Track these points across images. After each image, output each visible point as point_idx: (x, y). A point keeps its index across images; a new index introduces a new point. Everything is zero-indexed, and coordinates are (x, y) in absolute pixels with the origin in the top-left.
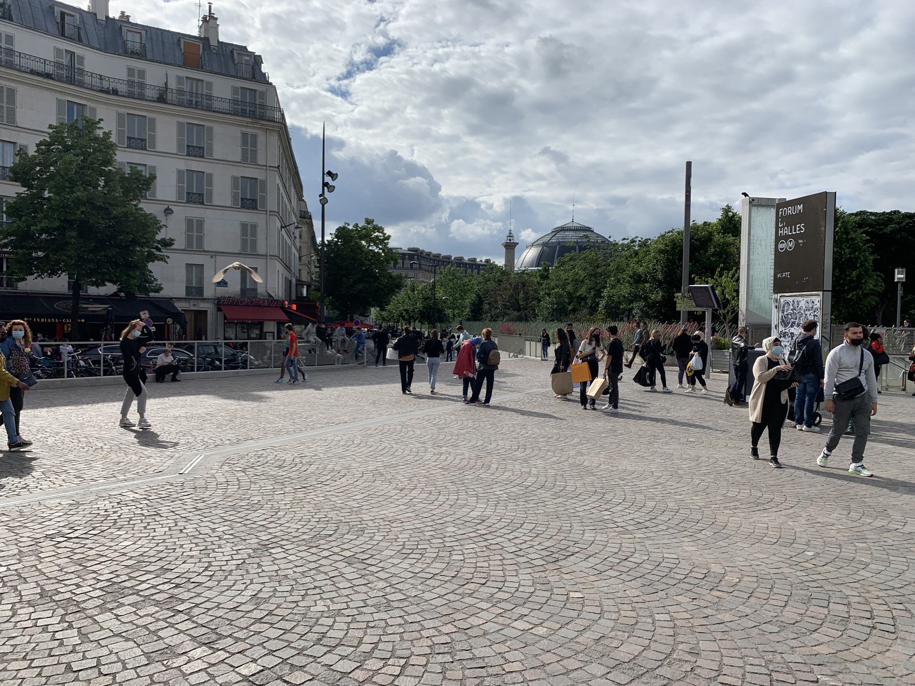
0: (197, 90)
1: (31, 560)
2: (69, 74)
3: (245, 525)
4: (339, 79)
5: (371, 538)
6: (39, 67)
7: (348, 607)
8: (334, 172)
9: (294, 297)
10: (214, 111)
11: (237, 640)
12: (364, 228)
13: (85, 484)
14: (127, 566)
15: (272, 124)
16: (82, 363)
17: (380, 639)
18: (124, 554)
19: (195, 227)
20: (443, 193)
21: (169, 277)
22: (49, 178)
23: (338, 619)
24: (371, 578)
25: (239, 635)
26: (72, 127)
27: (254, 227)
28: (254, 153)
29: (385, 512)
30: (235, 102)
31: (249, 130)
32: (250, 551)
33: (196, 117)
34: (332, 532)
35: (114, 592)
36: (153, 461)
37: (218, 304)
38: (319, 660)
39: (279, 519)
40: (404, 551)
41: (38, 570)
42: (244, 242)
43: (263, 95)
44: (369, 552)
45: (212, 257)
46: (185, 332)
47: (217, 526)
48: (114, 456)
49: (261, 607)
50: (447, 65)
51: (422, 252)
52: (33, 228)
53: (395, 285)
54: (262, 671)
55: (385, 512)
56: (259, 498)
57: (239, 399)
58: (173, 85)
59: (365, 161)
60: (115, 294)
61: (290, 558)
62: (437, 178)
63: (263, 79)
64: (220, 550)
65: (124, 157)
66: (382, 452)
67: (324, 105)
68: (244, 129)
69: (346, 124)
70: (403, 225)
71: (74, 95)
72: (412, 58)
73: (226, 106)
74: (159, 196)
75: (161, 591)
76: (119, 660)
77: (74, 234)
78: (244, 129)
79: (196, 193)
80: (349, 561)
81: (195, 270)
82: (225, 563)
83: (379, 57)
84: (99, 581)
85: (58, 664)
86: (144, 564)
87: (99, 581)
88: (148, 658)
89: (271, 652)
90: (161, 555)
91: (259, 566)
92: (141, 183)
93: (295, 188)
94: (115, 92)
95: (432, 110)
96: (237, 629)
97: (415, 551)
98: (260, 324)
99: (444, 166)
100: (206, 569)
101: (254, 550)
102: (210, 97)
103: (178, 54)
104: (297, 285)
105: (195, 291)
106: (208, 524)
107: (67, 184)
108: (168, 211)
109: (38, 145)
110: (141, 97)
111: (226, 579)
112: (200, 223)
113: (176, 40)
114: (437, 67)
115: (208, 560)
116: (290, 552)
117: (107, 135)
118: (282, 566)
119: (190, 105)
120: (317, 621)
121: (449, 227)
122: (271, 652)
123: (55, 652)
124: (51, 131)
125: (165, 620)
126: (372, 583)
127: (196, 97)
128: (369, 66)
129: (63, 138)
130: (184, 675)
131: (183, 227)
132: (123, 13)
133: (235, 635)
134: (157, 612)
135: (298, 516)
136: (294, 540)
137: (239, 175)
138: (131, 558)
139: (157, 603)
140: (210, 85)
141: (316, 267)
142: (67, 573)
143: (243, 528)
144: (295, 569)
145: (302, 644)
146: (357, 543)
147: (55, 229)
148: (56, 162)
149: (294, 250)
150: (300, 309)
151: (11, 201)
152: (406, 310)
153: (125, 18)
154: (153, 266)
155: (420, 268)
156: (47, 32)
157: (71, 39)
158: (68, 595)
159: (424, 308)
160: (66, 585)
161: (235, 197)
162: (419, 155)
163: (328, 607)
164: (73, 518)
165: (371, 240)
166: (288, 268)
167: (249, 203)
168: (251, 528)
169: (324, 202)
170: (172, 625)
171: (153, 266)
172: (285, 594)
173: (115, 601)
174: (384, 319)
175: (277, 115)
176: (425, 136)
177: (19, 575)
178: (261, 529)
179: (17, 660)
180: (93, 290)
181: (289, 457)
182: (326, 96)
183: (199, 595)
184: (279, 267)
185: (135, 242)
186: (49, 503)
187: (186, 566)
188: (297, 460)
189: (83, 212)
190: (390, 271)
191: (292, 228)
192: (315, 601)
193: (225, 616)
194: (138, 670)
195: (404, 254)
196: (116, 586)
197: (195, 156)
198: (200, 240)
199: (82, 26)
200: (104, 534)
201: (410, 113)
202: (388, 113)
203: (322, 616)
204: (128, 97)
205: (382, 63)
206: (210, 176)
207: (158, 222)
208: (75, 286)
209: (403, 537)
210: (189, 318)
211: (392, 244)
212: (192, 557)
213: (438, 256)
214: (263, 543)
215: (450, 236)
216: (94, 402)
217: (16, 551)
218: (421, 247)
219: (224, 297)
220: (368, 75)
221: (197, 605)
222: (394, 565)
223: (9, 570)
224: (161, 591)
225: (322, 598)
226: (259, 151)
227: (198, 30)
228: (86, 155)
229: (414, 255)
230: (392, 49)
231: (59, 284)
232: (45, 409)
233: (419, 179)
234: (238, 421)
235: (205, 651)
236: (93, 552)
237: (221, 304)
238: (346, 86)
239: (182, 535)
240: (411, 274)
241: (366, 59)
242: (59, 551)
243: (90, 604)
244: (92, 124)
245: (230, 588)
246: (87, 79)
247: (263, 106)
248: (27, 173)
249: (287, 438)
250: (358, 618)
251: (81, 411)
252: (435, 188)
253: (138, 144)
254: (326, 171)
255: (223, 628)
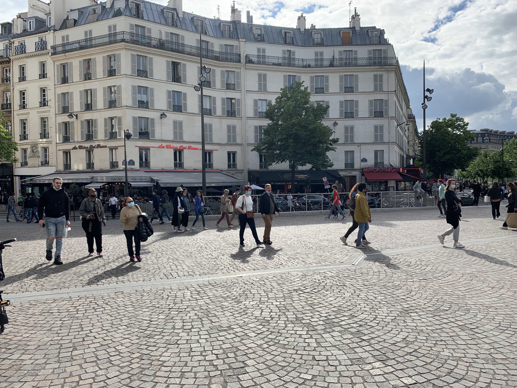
0: (349, 56)
1: (289, 301)
2: (289, 61)
3: (393, 297)
4: (430, 32)
5: (475, 316)
6: (276, 61)
7: (465, 357)
8: (431, 89)
9: (405, 166)
10: (359, 66)
11: (398, 362)
12: (449, 121)
13: (307, 266)
14: (333, 311)
15: (391, 67)
16: (297, 204)
17: (491, 381)
18: (331, 304)
19: (349, 131)
20: (506, 90)
21: (336, 159)
22: (281, 114)
23: (459, 362)
24: (479, 341)
25: (399, 359)
26: (291, 88)
27: (382, 127)
28: (381, 86)
29: (483, 301)
30: (370, 58)
31: (378, 73)
32: (398, 313)
33: (348, 71)
34: (447, 309)
35: (329, 324)
36: (337, 256)
37: (362, 172)
38: (451, 385)
39: (413, 296)
40: (501, 328)
41: (293, 306)
42: (376, 136)
43: (385, 51)
44: (475, 324)
45: (358, 146)
46: (345, 188)
47: (377, 296)
48: (318, 252)
49: (409, 346)
50: (507, 6)
51: (491, 131)
52: (275, 140)
53: (473, 154)
54: (416, 383)
55: (483, 301)
56: (399, 283)
57: (378, 225)
58: (337, 56)
59: (448, 78)
60: (311, 169)
61: (423, 320)
62: (501, 81)
63: (385, 43)
64: (380, 309)
65: (314, 99)
66: (474, 262)
67: (420, 50)
68: (375, 73)
69: (434, 58)
70: (475, 116)
71: (290, 71)
72: (480, 7)
73: (365, 62)
74: (156, 107)
75: (352, 327)
76: (337, 360)
77: (292, 141)
78: (375, 73)
79: (349, 112)
80: (462, 328)
81: (350, 154)
82: (384, 317)
83: (456, 12)
84: (321, 316)
85: (309, 355)
86: (342, 311)
87: (321, 316)
88: (352, 362)
89: (420, 374)
90: (349, 308)
91: (405, 322)
92: (322, 110)
93: (405, 101)
94: (309, 66)
95: (496, 37)
96: (397, 356)
97: (509, 329)
98: (386, 182)
99: (506, 72)
100: (375, 319)
101: (400, 312)
102: (356, 59)
103: (339, 39)
104: (406, 158)
105: (350, 166)
106: (372, 294)
107: (289, 117)
108: (335, 124)
109: (276, 99)
110: (322, 66)
111: (386, 326)
112: (352, 128)
114: (499, 9)
115: (375, 314)
116: (422, 316)
117: (306, 89)
118: (419, 324)
119: (346, 65)
120: (446, 361)
121: (512, 112)
122: (420, 374)
123: (307, 348)
124: (281, 91)
125: (357, 343)
126: (480, 344)
128: (449, 19)
129: (287, 94)
130: (372, 375)
131: (343, 131)
132: (312, 25)
133: (397, 359)
134: (352, 338)
135: (424, 296)
136: (424, 310)
137: (171, 89)
138: (335, 307)
139: (352, 333)
140: (356, 52)
141: (419, 147)
142: (306, 310)
143: (392, 299)
144: (427, 327)
145: (439, 373)
146: (466, 317)
147: (284, 139)
148: (284, 106)
149: (405, 138)
150: (409, 174)
151: (265, 128)
152: (480, 170)
153: (313, 27)
154: (329, 154)
155: (490, 142)
156: (279, 43)
157: (289, 44)
158: (308, 321)
159: (495, 168)
160: (306, 316)
161: (370, 112)
162: (488, 68)
163: (452, 354)
164: (305, 282)
165: (458, 127)
166: (401, 149)
167: (379, 114)
168: (397, 300)
169: (425, 107)
170: (361, 347)
171: (329, 154)
172: (423, 341)
173: (331, 328)
174: (464, 176)
175: (394, 61)
176: (491, 55)
177: (285, 307)
178: (402, 300)
179: (290, 349)
180: (300, 168)
181: (413, 261)
182: (421, 44)
183: (373, 333)
184: (396, 148)
185: (320, 142)
186: (293, 273)
187: (364, 316)
188: (418, 263)
189: (296, 130)
190: (469, 145)
191: (403, 125)
192: (443, 349)
193: (389, 347)
194: (347, 367)
195: (478, 134)
196: (330, 321)
197: (349, 92)
198: (352, 137)
199: (294, 37)
200: (320, 292)
201: (480, 42)
202: (464, 46)
203: (449, 359)
205: (458, 15)
206: (357, 102)
207: (331, 130)
208: (293, 167)
209: (499, 318)
210: (347, 180)
211: (469, 128)
212: (366, 311)
213: (504, 132)
214: (405, 309)
215: (512, 118)
216: (304, 224)
217: (282, 296)
219: (366, 168)
220: (449, 25)
221: (373, 338)
222: (494, 336)
223: (280, 304)
224: (352, 327)
225: (447, 348)
226: (384, 84)
227: (349, 23)
228: (297, 100)
229: (485, 133)
230: (465, 5)
231: (285, 166)
232: (284, 227)
233: (487, 84)
234: (379, 238)
235: (381, 365)
236: (316, 301)
237: (363, 172)
238: (434, 35)
239: (359, 298)
240: (483, 146)
241: (447, 16)
242: (301, 298)
243: (319, 328)
244: (299, 84)
245: (389, 332)
246: (297, 62)
247: (386, 58)
248: (271, 114)
249: (409, 249)
250: (474, 365)
251: (299, 229)
252: (500, 88)
253: (320, 90)
254: (426, 89)
255: (389, 354)
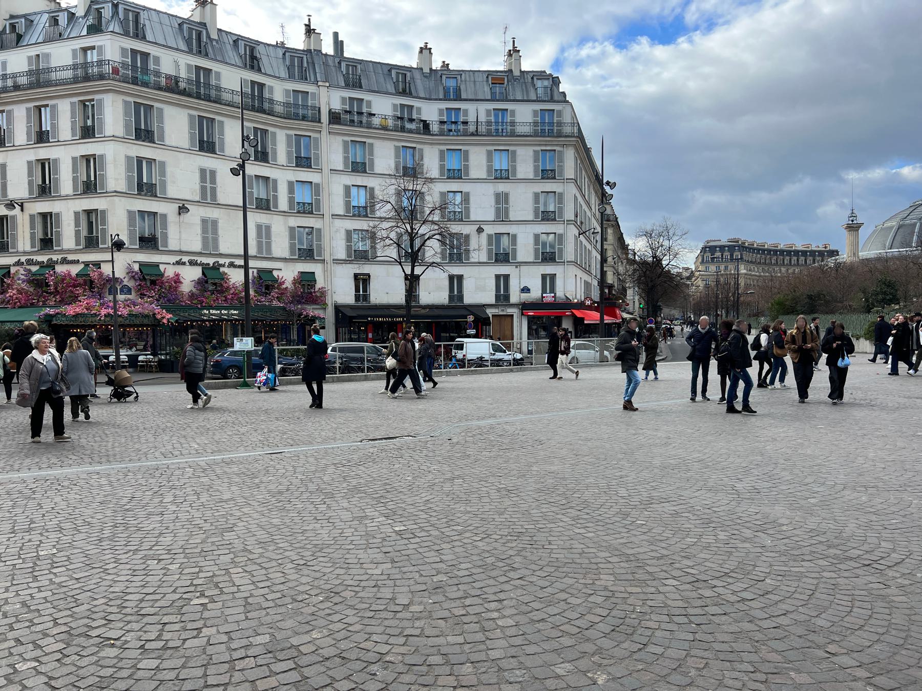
58: (483, 118)
113: (386, 71)
127: (502, 125)
140: (513, 113)
204: (440, 135)
218: (743, 238)
